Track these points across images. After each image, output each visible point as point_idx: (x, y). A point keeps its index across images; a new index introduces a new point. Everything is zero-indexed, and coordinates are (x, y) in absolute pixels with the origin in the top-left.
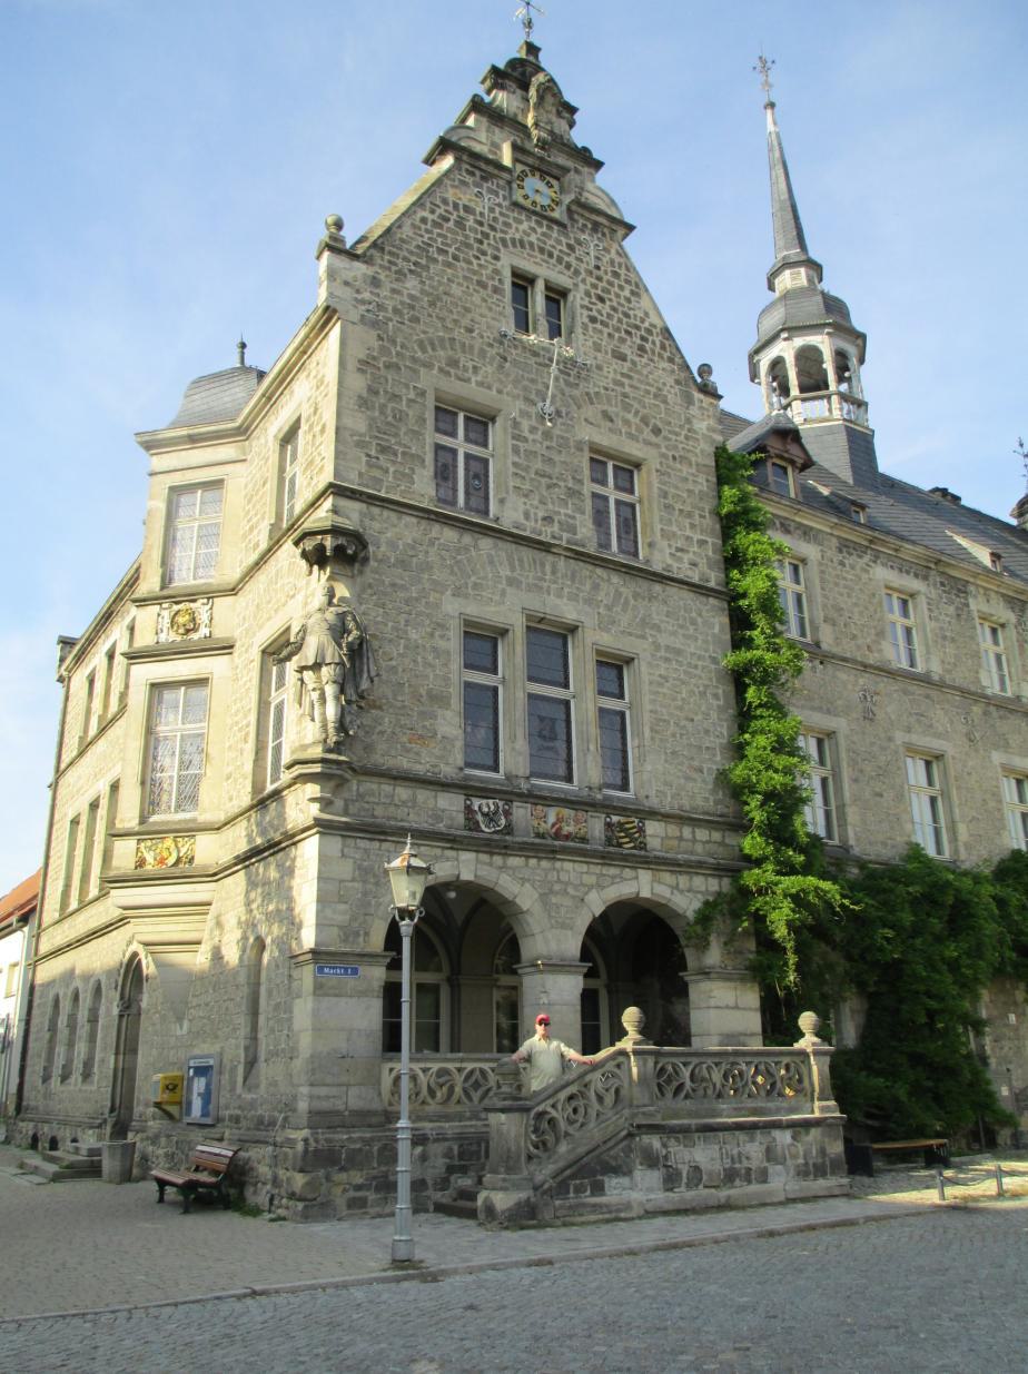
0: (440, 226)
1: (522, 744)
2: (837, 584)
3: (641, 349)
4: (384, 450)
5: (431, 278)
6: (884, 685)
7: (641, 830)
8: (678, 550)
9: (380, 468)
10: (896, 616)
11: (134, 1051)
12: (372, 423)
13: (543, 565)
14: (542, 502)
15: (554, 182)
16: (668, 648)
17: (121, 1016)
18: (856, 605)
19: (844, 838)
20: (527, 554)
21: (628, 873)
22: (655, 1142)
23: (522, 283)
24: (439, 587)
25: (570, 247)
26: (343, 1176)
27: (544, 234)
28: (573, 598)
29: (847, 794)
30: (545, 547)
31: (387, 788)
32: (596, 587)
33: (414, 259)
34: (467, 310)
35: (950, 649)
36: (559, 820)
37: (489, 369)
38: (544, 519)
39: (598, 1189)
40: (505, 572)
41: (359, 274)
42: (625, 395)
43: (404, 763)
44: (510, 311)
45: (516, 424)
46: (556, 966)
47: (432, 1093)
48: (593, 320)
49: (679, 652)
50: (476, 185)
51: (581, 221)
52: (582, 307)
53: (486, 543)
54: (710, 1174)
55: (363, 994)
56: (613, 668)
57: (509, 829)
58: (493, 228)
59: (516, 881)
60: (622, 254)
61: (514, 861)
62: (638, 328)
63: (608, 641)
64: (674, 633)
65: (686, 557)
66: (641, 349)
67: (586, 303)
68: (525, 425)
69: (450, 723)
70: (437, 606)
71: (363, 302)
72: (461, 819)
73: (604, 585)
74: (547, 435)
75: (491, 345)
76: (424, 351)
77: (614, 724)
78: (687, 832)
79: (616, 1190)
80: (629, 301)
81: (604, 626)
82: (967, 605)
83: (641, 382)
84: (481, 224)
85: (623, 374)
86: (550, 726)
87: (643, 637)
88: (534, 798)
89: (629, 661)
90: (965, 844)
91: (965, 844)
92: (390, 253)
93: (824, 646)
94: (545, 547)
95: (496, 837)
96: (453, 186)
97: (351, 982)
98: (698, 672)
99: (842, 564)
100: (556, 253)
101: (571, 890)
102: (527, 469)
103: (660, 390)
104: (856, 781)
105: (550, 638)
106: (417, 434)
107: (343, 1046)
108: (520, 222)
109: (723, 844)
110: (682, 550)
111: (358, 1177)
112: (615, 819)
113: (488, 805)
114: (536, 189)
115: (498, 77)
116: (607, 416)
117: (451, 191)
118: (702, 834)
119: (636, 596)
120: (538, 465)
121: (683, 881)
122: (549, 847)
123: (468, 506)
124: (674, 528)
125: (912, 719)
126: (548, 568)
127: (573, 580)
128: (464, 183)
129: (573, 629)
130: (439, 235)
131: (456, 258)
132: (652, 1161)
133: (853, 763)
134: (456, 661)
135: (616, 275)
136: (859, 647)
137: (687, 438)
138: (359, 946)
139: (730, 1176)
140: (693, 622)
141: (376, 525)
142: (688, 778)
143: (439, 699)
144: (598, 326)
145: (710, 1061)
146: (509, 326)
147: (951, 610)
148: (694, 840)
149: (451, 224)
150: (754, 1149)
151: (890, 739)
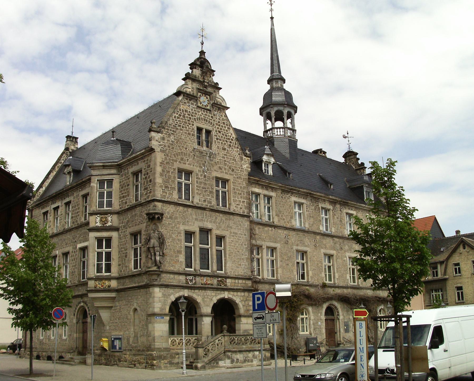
0: (178, 118)
1: (198, 262)
2: (280, 204)
3: (230, 146)
4: (166, 187)
5: (177, 135)
6: (292, 233)
7: (226, 281)
8: (237, 205)
9: (165, 192)
10: (297, 210)
11: (86, 332)
12: (163, 181)
13: (203, 214)
14: (203, 196)
15: (208, 97)
16: (234, 233)
17: (77, 323)
18: (285, 209)
19: (277, 277)
20: (199, 211)
21: (222, 292)
22: (229, 354)
23: (199, 130)
24: (179, 223)
25: (212, 117)
26: (163, 361)
27: (205, 115)
28: (211, 222)
29: (279, 265)
30: (204, 209)
31: (169, 275)
32: (216, 218)
33: (172, 129)
34: (186, 142)
35: (312, 220)
36: (207, 280)
37: (191, 159)
38: (204, 201)
39: (217, 363)
40: (194, 217)
41: (159, 137)
42: (225, 161)
43: (172, 268)
44: (196, 141)
45: (197, 175)
46: (207, 316)
47: (179, 344)
48: (217, 139)
49: (236, 233)
50: (188, 103)
51: (215, 108)
52: (215, 135)
53: (190, 210)
54: (241, 360)
55: (165, 323)
56: (220, 239)
57: (195, 283)
58: (192, 116)
59: (198, 296)
60: (226, 116)
61: (196, 291)
62: (229, 139)
63: (219, 232)
64: (235, 229)
65: (239, 206)
66: (230, 146)
67: (216, 134)
68: (200, 174)
69: (182, 258)
70: (179, 228)
71: (160, 145)
72: (184, 281)
73: (218, 218)
74: (205, 176)
75: (191, 152)
76: (175, 157)
77: (219, 253)
78: (237, 281)
79: (221, 363)
80: (227, 131)
81: (218, 229)
82: (318, 205)
83: (229, 156)
84: (189, 115)
85: (225, 155)
86: (204, 254)
87: (228, 230)
88: (201, 275)
89: (224, 237)
90: (311, 277)
91: (311, 277)
92: (167, 129)
93: (275, 223)
94: (204, 209)
95: (193, 285)
96: (182, 105)
97: (162, 320)
98: (241, 239)
99: (282, 197)
100: (208, 120)
101: (209, 297)
102: (200, 187)
103: (234, 157)
104: (281, 261)
105: (205, 232)
106: (173, 181)
107: (161, 334)
108: (199, 112)
109: (245, 283)
110: (237, 205)
111: (166, 361)
112: (220, 279)
113: (191, 278)
114: (204, 100)
115: (192, 66)
116: (220, 168)
117: (182, 106)
118: (240, 281)
119: (226, 219)
120: (202, 185)
121: (235, 293)
122: (203, 288)
123: (185, 199)
124: (237, 199)
125: (299, 242)
126: (205, 214)
127: (211, 217)
128: (185, 103)
129: (210, 230)
130: (179, 121)
131: (183, 127)
132: (229, 358)
133: (281, 256)
134: (183, 241)
135: (224, 123)
136: (285, 222)
137: (241, 171)
138: (164, 312)
139: (245, 361)
140: (240, 225)
141: (165, 208)
142: (237, 267)
143: (179, 252)
144: (219, 141)
145: (241, 337)
146: (196, 146)
147: (313, 207)
148: (238, 283)
149: (182, 117)
150: (250, 355)
151: (292, 248)
